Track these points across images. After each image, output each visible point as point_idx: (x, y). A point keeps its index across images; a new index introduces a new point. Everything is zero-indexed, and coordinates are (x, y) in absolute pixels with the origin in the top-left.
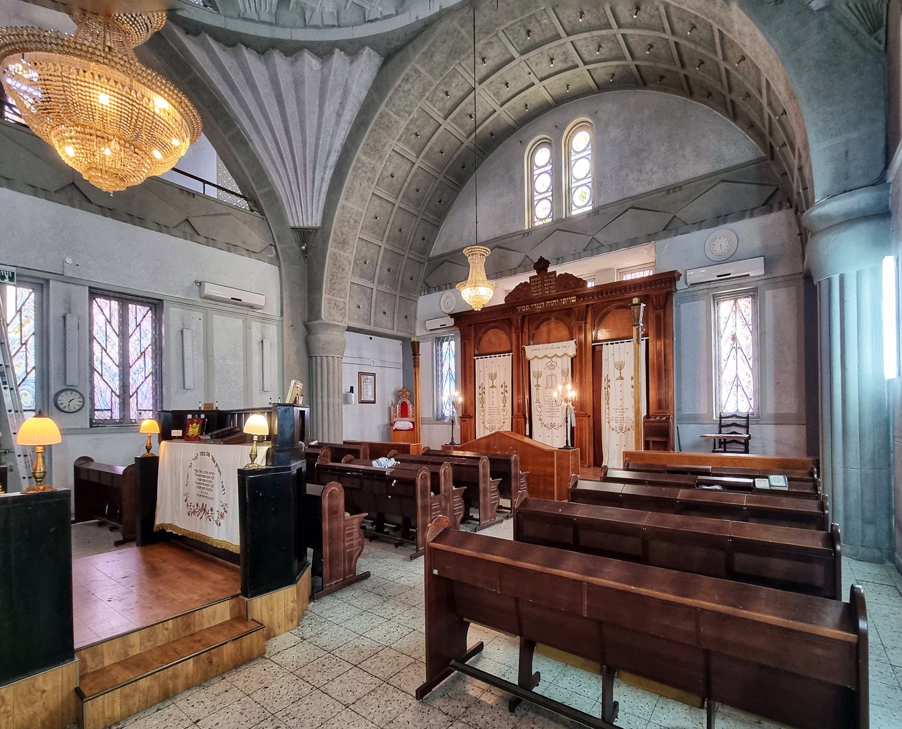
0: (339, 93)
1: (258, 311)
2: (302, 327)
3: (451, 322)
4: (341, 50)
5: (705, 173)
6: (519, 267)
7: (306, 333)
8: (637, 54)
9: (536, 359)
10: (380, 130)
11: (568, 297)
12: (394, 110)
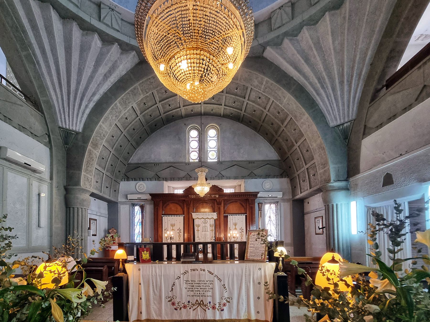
0: (110, 65)
1: (37, 174)
2: (63, 189)
3: (149, 197)
4: (119, 45)
7: (65, 193)
8: (247, 111)
10: (131, 95)
12: (141, 88)
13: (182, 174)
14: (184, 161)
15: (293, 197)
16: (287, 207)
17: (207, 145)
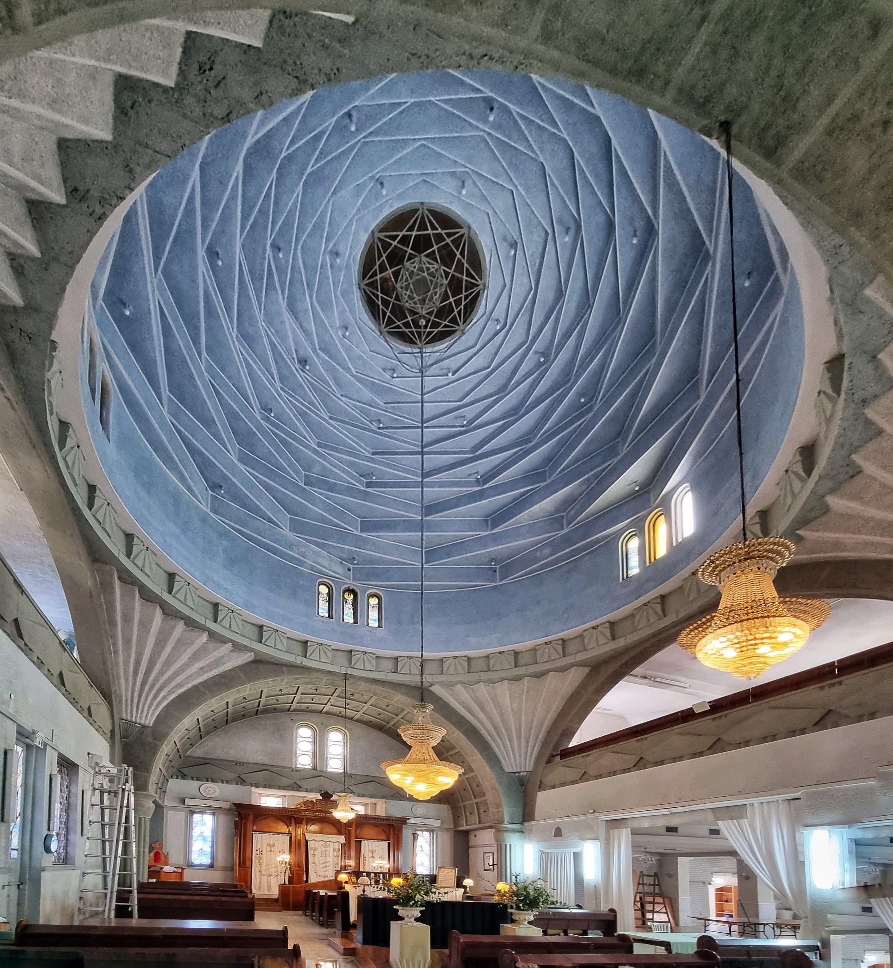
13: (285, 781)
14: (288, 765)
15: (455, 827)
16: (446, 839)
17: (327, 751)
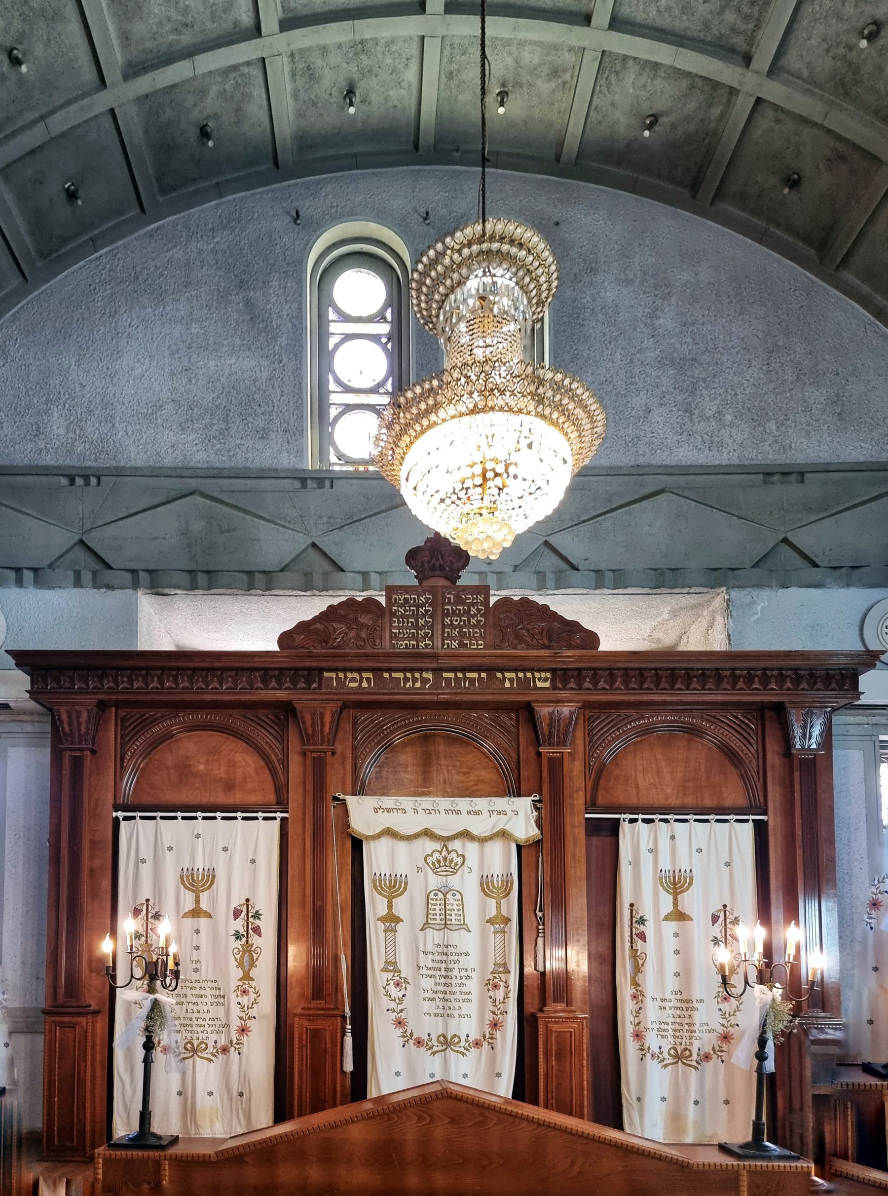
5: (862, 459)
6: (282, 570)
9: (385, 841)
11: (524, 670)
